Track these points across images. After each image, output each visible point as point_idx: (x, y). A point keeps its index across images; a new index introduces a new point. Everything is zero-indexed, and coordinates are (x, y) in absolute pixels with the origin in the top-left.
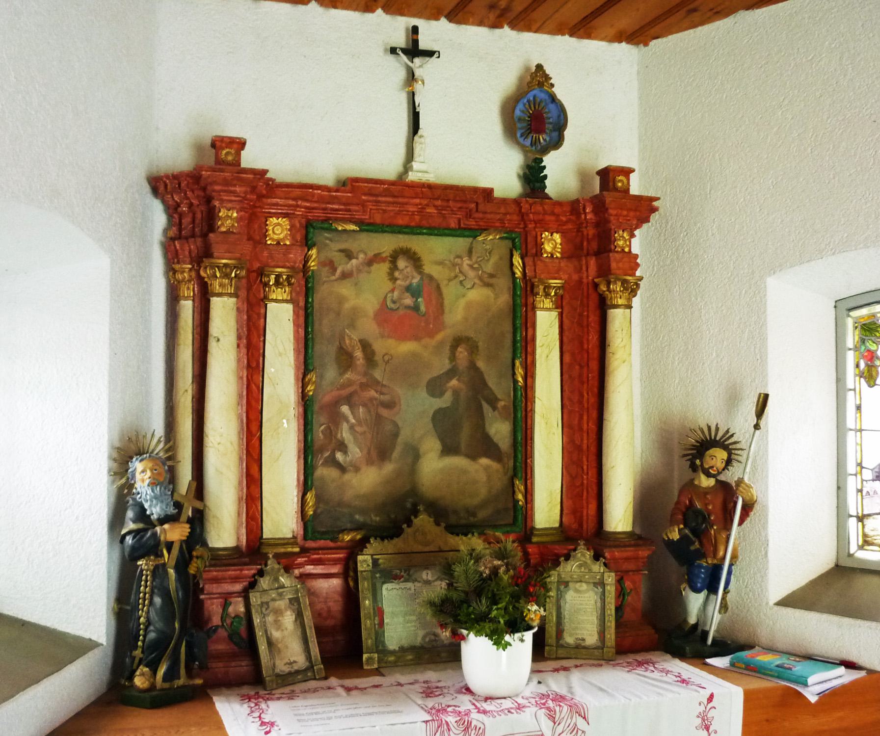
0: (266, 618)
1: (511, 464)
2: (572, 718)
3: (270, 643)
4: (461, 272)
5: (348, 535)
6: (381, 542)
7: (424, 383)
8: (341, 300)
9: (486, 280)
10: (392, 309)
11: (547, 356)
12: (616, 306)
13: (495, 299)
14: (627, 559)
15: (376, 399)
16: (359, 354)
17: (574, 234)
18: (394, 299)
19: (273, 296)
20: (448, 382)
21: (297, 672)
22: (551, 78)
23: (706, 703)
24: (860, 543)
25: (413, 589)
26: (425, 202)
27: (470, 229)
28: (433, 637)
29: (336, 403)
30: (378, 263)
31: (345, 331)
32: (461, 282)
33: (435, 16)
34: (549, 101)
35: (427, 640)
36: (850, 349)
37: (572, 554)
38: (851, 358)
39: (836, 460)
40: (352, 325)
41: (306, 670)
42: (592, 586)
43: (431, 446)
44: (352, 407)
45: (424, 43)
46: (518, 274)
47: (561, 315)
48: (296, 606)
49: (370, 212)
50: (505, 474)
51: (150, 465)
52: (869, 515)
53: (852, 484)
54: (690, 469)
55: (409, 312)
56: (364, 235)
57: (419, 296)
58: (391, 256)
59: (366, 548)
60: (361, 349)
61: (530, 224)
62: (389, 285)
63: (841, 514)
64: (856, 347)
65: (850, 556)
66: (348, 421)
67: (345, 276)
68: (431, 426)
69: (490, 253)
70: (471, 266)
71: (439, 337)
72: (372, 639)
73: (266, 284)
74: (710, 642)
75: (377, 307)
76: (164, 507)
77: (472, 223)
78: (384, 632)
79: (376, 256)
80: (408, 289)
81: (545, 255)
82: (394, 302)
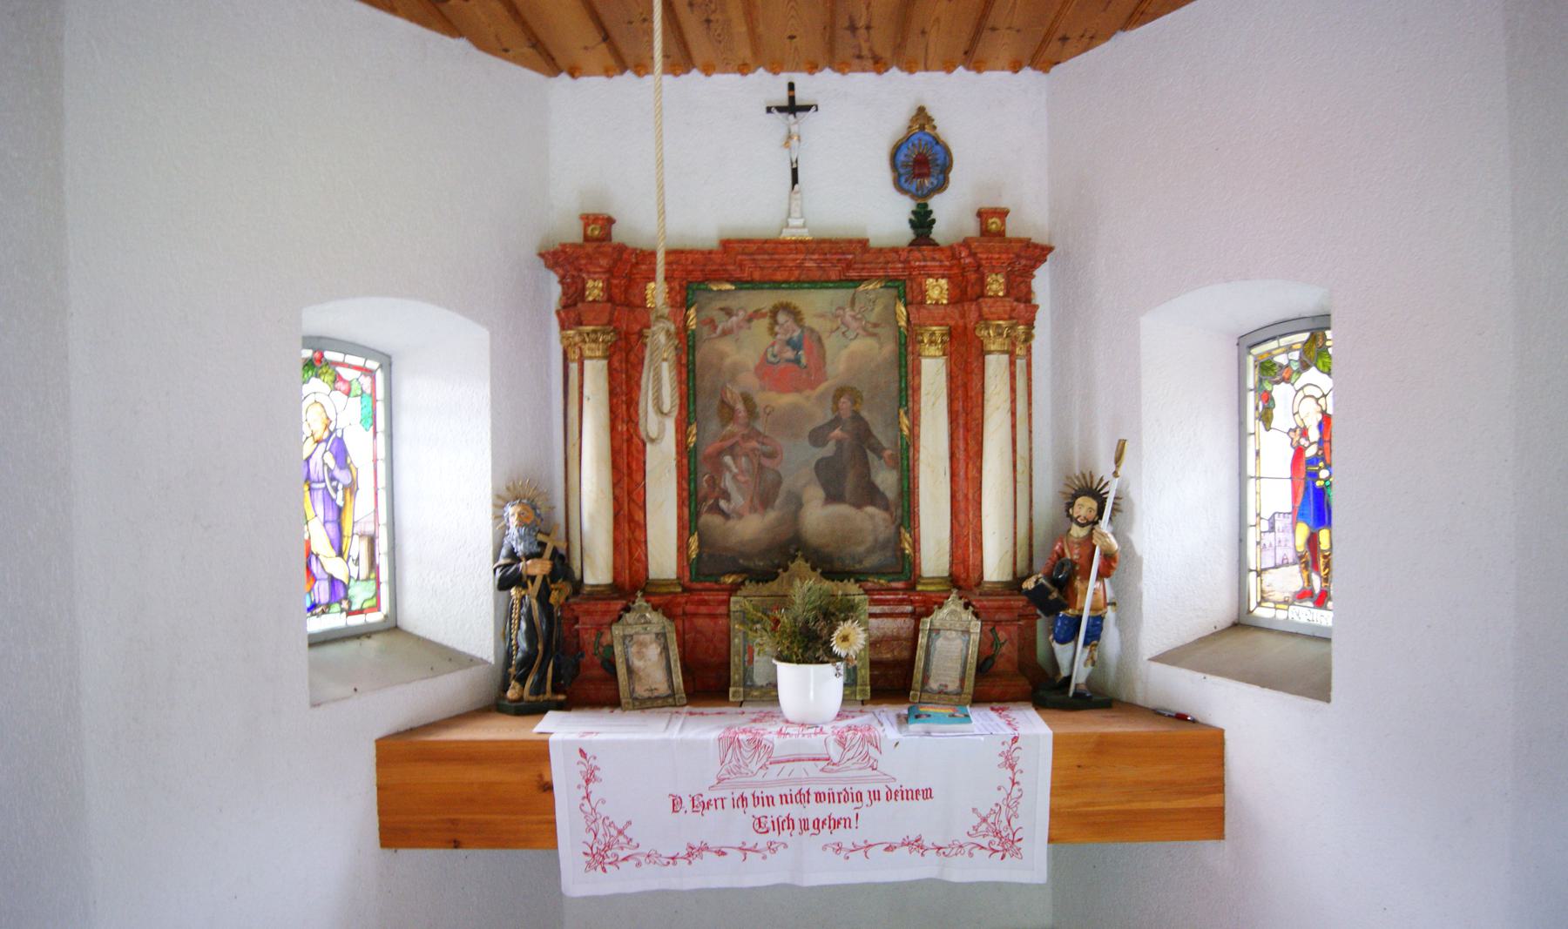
0: (629, 649)
1: (899, 512)
2: (863, 747)
3: (630, 671)
5: (729, 577)
6: (755, 585)
7: (807, 434)
8: (722, 356)
9: (871, 330)
10: (772, 363)
12: (990, 352)
13: (880, 348)
14: (999, 608)
15: (758, 450)
16: (740, 406)
19: (927, 353)
21: (657, 698)
22: (933, 120)
23: (1010, 743)
24: (1259, 599)
26: (802, 257)
30: (758, 318)
32: (843, 333)
33: (813, 68)
34: (934, 143)
36: (1251, 390)
37: (946, 601)
38: (1251, 398)
39: (1237, 510)
40: (733, 379)
41: (668, 696)
42: (960, 633)
43: (814, 497)
44: (734, 458)
45: (801, 99)
46: (903, 323)
47: (610, 365)
48: (662, 640)
50: (893, 523)
51: (519, 509)
52: (1266, 569)
53: (1252, 536)
55: (790, 365)
56: (742, 293)
58: (771, 311)
62: (769, 340)
63: (1242, 568)
64: (1255, 388)
65: (1250, 612)
66: (731, 471)
67: (725, 333)
68: (814, 474)
69: (874, 302)
70: (854, 317)
71: (822, 388)
72: (739, 674)
74: (1071, 694)
75: (757, 361)
77: (852, 274)
78: (753, 668)
80: (789, 342)
81: (929, 302)
82: (775, 356)
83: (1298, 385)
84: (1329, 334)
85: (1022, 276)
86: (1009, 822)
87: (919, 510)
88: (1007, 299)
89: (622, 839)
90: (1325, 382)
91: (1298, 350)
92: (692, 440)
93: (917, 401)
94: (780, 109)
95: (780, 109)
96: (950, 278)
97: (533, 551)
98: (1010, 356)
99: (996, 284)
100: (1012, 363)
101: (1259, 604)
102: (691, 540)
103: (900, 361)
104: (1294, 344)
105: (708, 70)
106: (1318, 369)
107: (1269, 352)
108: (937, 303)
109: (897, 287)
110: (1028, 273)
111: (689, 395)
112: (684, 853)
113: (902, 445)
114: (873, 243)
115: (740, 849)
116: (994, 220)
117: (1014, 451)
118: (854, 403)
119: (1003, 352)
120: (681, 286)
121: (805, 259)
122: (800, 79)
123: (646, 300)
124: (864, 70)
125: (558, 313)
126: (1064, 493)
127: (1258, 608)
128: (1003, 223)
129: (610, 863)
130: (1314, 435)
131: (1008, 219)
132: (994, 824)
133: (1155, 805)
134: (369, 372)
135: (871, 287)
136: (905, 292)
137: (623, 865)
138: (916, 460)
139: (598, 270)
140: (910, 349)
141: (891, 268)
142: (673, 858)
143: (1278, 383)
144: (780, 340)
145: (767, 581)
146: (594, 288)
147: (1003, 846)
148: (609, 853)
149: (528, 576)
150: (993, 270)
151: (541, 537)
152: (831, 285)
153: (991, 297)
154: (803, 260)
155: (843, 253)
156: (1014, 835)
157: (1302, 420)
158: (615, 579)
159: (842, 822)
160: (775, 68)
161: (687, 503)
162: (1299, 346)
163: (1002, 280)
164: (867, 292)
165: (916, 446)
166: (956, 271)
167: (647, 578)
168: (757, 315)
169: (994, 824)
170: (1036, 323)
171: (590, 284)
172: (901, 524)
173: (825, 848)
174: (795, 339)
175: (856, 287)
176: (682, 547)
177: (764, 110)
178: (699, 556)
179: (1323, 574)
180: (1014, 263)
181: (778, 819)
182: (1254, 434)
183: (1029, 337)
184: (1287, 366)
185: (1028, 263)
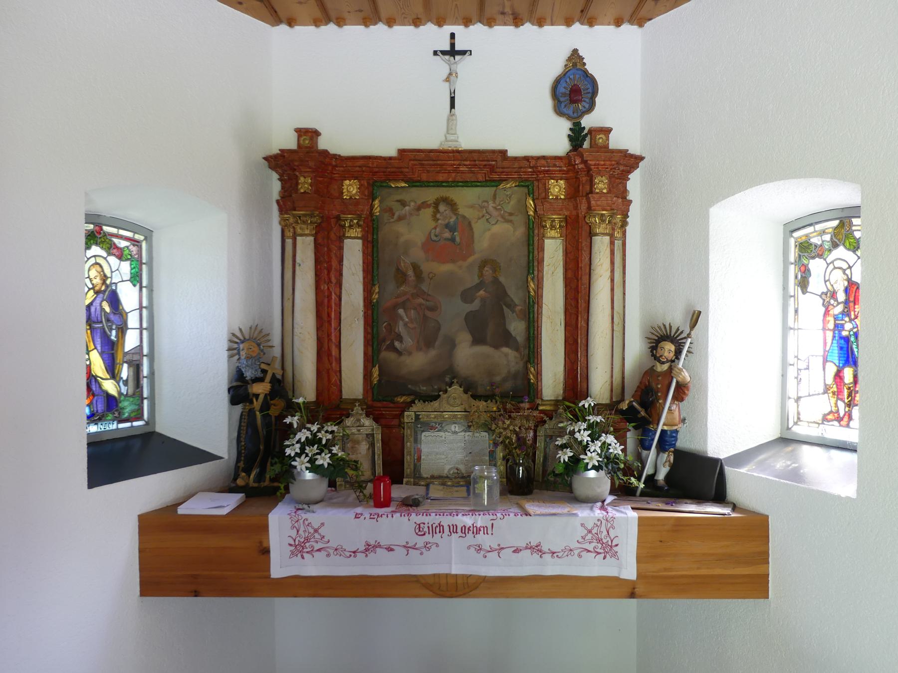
1: (527, 352)
5: (401, 398)
11: (553, 273)
12: (596, 235)
13: (514, 232)
15: (423, 305)
16: (410, 273)
17: (574, 180)
18: (436, 233)
20: (477, 293)
25: (444, 436)
27: (494, 181)
28: (456, 471)
29: (395, 307)
31: (400, 257)
32: (487, 219)
33: (467, 22)
35: (451, 472)
38: (792, 269)
43: (464, 339)
46: (531, 213)
47: (315, 240)
49: (418, 173)
56: (413, 190)
58: (434, 203)
59: (412, 407)
60: (412, 270)
61: (541, 174)
62: (433, 224)
66: (403, 320)
67: (400, 219)
70: (495, 208)
73: (344, 227)
76: (253, 372)
77: (495, 176)
79: (423, 203)
80: (447, 226)
83: (829, 260)
84: (855, 221)
85: (620, 179)
86: (608, 533)
87: (541, 351)
88: (609, 195)
89: (317, 535)
90: (850, 257)
91: (830, 233)
92: (375, 296)
93: (540, 270)
94: (444, 53)
96: (567, 179)
97: (257, 376)
99: (601, 184)
100: (612, 243)
101: (796, 424)
103: (529, 240)
104: (826, 229)
105: (390, 23)
106: (845, 247)
107: (807, 235)
108: (557, 198)
109: (528, 186)
110: (624, 177)
111: (373, 264)
112: (362, 548)
113: (529, 303)
114: (510, 154)
115: (405, 547)
116: (601, 136)
117: (613, 308)
118: (494, 271)
120: (368, 183)
121: (460, 165)
123: (343, 193)
124: (505, 24)
125: (278, 202)
127: (795, 426)
129: (307, 552)
130: (841, 297)
131: (612, 135)
132: (597, 534)
133: (718, 571)
135: (508, 186)
136: (533, 189)
137: (316, 554)
138: (540, 313)
139: (308, 170)
140: (536, 232)
141: (524, 172)
142: (354, 552)
143: (813, 258)
144: (441, 224)
145: (431, 401)
146: (305, 183)
147: (604, 550)
148: (307, 545)
150: (599, 173)
151: (263, 366)
153: (597, 193)
154: (458, 165)
155: (488, 161)
156: (612, 541)
157: (832, 286)
158: (317, 398)
159: (482, 529)
160: (440, 22)
161: (371, 343)
162: (831, 230)
164: (505, 189)
165: (540, 303)
166: (572, 175)
167: (341, 398)
168: (424, 205)
169: (597, 534)
170: (629, 214)
171: (302, 179)
172: (529, 361)
173: (469, 547)
175: (497, 186)
176: (367, 375)
177: (432, 53)
178: (379, 381)
179: (846, 401)
180: (615, 169)
181: (432, 525)
182: (794, 296)
183: (624, 224)
184: (821, 246)
185: (625, 168)
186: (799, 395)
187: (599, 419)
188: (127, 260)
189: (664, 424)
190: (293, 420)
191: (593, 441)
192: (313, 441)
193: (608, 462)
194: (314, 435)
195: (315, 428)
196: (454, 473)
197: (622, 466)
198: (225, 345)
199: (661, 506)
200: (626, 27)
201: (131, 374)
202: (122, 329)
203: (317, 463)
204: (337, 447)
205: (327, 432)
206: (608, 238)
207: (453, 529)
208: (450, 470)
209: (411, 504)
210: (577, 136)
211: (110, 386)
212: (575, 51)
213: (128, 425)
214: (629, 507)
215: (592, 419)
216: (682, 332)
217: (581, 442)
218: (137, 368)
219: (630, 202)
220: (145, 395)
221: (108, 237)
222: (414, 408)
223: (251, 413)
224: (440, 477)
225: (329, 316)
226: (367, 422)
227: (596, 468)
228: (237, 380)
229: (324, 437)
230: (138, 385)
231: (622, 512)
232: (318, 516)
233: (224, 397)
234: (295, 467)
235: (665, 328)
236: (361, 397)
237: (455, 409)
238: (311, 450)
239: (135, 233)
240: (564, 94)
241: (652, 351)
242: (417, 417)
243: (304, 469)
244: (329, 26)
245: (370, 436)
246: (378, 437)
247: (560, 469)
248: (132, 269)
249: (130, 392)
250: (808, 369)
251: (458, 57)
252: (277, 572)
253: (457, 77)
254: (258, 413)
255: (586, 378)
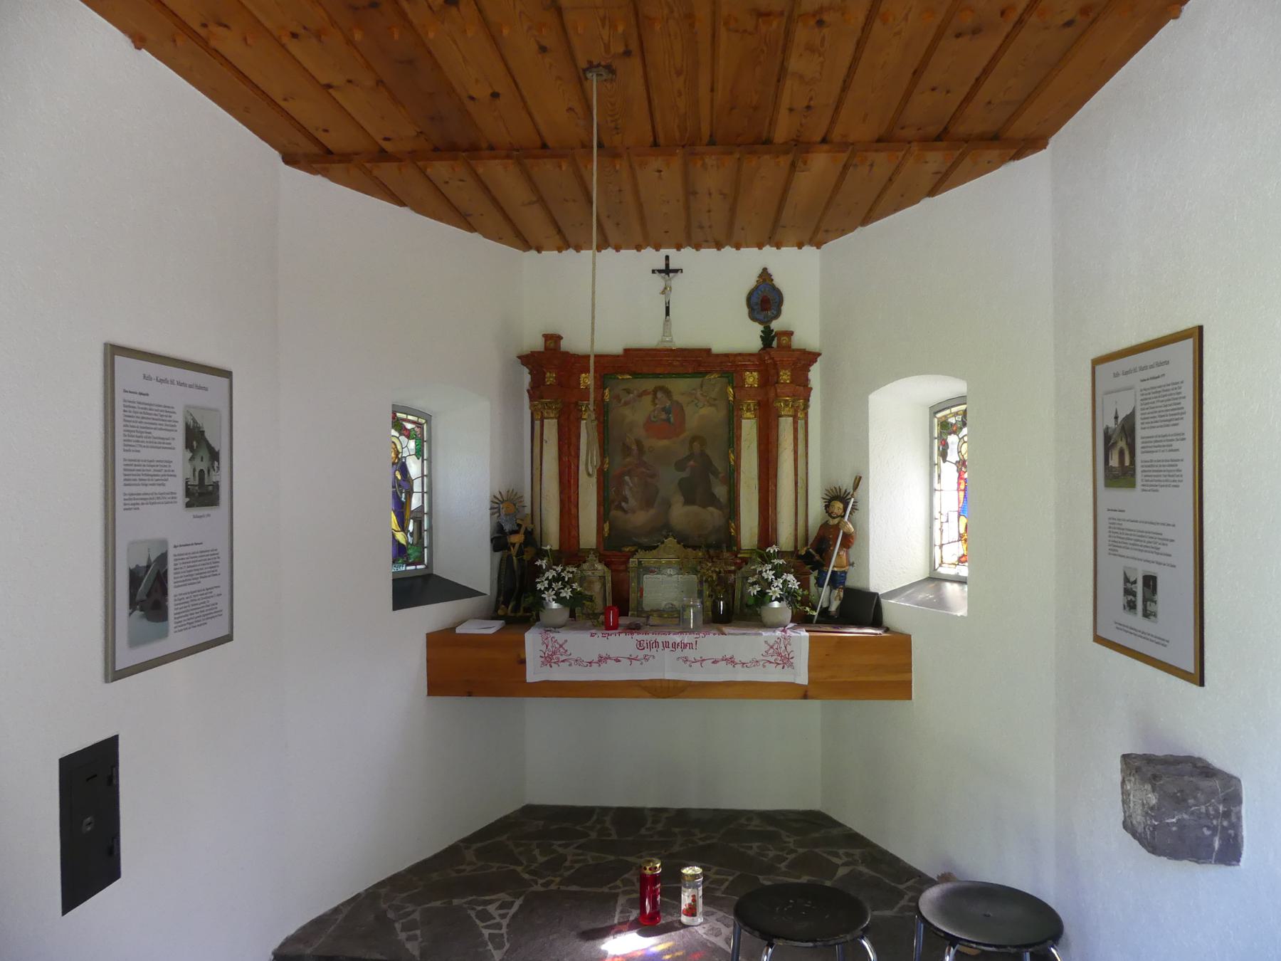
4: (696, 398)
12: (781, 416)
16: (634, 447)
26: (671, 359)
32: (696, 404)
35: (667, 607)
36: (936, 438)
43: (677, 501)
46: (731, 398)
54: (217, 450)
57: (670, 414)
58: (653, 391)
66: (628, 485)
67: (626, 404)
70: (702, 394)
73: (581, 410)
77: (702, 369)
80: (664, 409)
83: (961, 436)
89: (562, 650)
92: (606, 466)
93: (739, 445)
94: (660, 271)
95: (660, 271)
98: (794, 418)
99: (785, 376)
100: (795, 423)
102: (605, 525)
105: (618, 249)
107: (945, 416)
109: (728, 377)
116: (785, 338)
117: (796, 474)
119: (791, 416)
122: (672, 252)
123: (580, 384)
125: (528, 391)
126: (824, 499)
128: (790, 340)
129: (555, 663)
133: (872, 678)
134: (419, 425)
135: (712, 377)
137: (561, 664)
140: (735, 414)
142: (590, 663)
143: (950, 434)
145: (651, 550)
146: (550, 378)
149: (511, 544)
151: (519, 522)
152: (688, 376)
153: (782, 383)
158: (560, 548)
163: (789, 373)
168: (645, 393)
171: (548, 374)
174: (667, 407)
175: (704, 377)
176: (600, 530)
178: (609, 534)
182: (937, 464)
183: (806, 407)
186: (943, 543)
187: (781, 562)
188: (413, 439)
189: (834, 567)
190: (543, 563)
191: (776, 579)
192: (558, 578)
193: (788, 595)
194: (559, 574)
195: (559, 569)
196: (669, 608)
197: (799, 598)
198: (487, 505)
199: (829, 629)
200: (807, 249)
201: (416, 527)
202: (410, 493)
203: (562, 595)
204: (576, 584)
205: (568, 572)
206: (791, 419)
207: (666, 645)
208: (666, 605)
209: (633, 628)
210: (767, 336)
211: (400, 537)
212: (765, 270)
213: (413, 567)
214: (804, 630)
215: (776, 561)
216: (849, 493)
217: (768, 579)
218: (419, 523)
219: (811, 389)
220: (425, 545)
221: (401, 421)
222: (638, 556)
223: (510, 557)
224: (658, 611)
225: (569, 481)
226: (600, 567)
227: (779, 600)
228: (498, 533)
229: (567, 576)
230: (420, 537)
231: (797, 633)
232: (560, 636)
233: (487, 545)
234: (544, 599)
235: (829, 492)
236: (595, 547)
237: (671, 556)
238: (556, 586)
239: (419, 418)
240: (757, 304)
241: (826, 509)
242: (640, 563)
243: (551, 600)
244: (568, 251)
245: (603, 578)
246: (609, 578)
247: (751, 602)
248: (416, 446)
249: (415, 542)
250: (947, 521)
251: (671, 275)
252: (531, 677)
253: (671, 291)
254: (514, 558)
255: (775, 530)
